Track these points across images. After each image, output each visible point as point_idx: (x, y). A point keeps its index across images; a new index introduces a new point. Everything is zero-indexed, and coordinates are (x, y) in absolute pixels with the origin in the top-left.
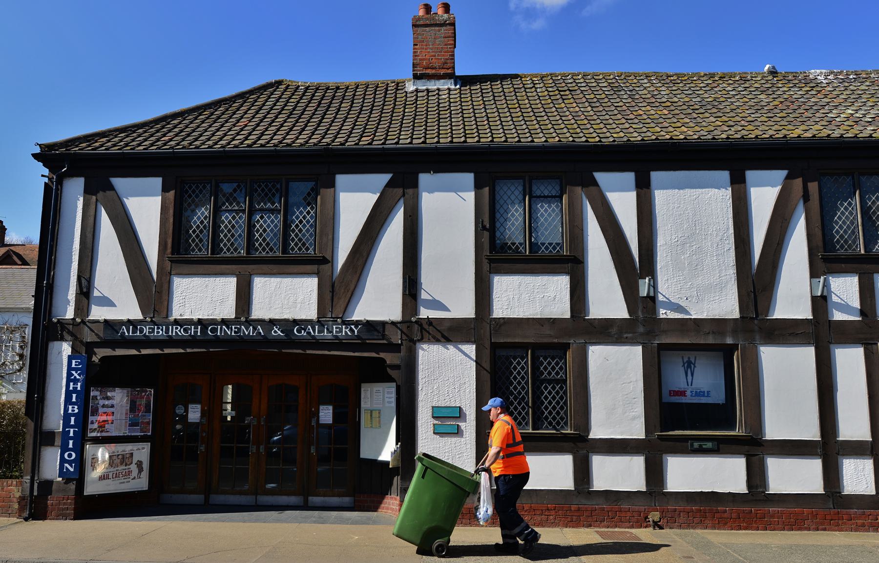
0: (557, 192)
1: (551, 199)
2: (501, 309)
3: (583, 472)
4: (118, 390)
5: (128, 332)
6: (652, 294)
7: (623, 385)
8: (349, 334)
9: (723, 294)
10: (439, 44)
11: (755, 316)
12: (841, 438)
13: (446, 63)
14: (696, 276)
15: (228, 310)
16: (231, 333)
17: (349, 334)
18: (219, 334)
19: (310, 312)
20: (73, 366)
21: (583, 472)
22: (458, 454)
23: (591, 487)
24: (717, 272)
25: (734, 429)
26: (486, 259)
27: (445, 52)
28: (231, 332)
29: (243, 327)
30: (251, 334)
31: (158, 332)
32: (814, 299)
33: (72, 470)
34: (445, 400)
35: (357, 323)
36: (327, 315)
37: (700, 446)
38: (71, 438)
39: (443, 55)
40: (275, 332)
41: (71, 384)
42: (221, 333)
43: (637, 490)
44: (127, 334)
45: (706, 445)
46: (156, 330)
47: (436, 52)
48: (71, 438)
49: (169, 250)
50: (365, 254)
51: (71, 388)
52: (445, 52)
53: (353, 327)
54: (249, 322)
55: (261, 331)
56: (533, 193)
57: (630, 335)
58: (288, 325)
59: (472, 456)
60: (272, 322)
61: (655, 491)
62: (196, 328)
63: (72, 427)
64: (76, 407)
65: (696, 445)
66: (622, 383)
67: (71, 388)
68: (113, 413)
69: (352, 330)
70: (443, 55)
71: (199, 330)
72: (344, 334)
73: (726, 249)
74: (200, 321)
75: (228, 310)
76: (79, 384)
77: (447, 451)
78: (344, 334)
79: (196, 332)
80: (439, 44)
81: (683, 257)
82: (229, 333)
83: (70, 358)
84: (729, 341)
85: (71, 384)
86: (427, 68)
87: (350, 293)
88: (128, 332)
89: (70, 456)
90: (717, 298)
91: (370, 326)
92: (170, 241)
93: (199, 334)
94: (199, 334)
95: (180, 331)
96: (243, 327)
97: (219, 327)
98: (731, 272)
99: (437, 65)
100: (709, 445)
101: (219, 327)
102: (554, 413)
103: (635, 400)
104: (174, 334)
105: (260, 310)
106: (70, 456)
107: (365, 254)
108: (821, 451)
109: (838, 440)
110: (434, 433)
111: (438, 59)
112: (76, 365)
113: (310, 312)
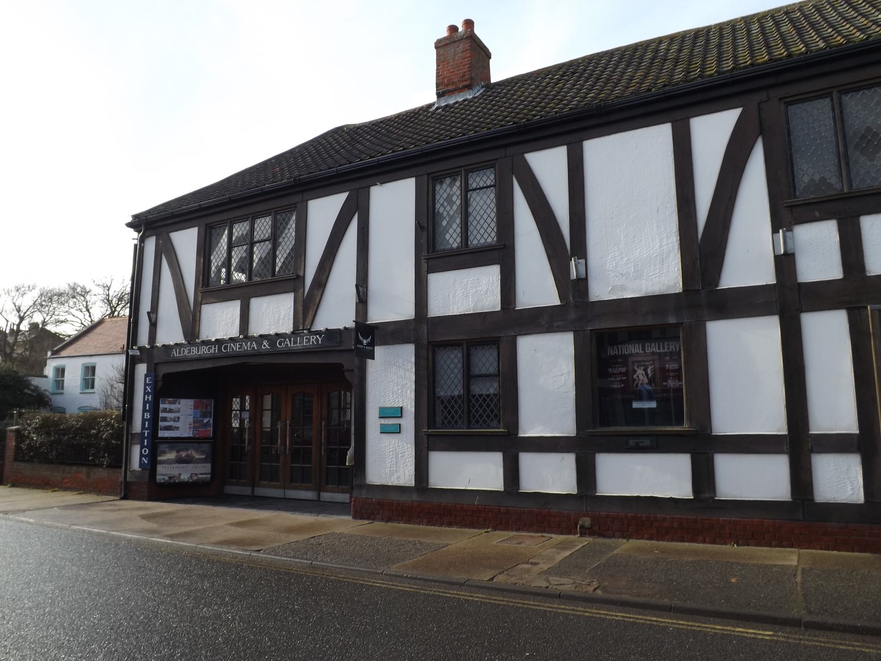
0: (492, 181)
1: (486, 189)
2: (437, 308)
3: (512, 473)
4: (183, 401)
5: (176, 354)
6: (583, 275)
7: (555, 378)
8: (315, 343)
9: (664, 265)
10: (458, 60)
11: (701, 288)
12: (814, 431)
13: (463, 76)
14: (634, 249)
15: (233, 331)
16: (236, 349)
17: (315, 343)
18: (228, 351)
19: (287, 327)
20: (147, 382)
21: (512, 473)
22: (400, 453)
23: (520, 488)
24: (658, 241)
25: (680, 422)
26: (424, 259)
27: (463, 66)
28: (236, 347)
29: (243, 343)
30: (249, 349)
31: (193, 352)
32: (778, 259)
33: (146, 462)
34: (390, 401)
35: (319, 333)
36: (299, 328)
37: (637, 444)
38: (146, 438)
39: (462, 69)
40: (264, 346)
41: (146, 396)
42: (230, 350)
43: (566, 493)
44: (289, 345)
45: (643, 442)
46: (192, 351)
47: (455, 68)
48: (146, 438)
49: (201, 285)
50: (328, 270)
51: (146, 399)
52: (463, 66)
53: (318, 336)
54: (252, 339)
55: (255, 346)
56: (469, 186)
57: (561, 323)
58: (273, 339)
59: (412, 455)
60: (262, 337)
61: (586, 495)
62: (215, 347)
63: (146, 429)
64: (149, 414)
65: (632, 442)
66: (553, 376)
67: (146, 399)
68: (179, 418)
69: (317, 340)
70: (462, 69)
71: (217, 348)
72: (311, 344)
73: (667, 214)
74: (218, 341)
75: (233, 331)
76: (150, 396)
77: (391, 450)
78: (311, 344)
79: (215, 350)
80: (458, 60)
81: (618, 230)
82: (235, 349)
83: (146, 376)
84: (672, 320)
85: (146, 396)
86: (447, 85)
87: (316, 306)
88: (176, 354)
89: (145, 451)
90: (658, 271)
91: (330, 334)
92: (201, 278)
93: (217, 352)
94: (217, 352)
95: (205, 350)
96: (243, 343)
97: (229, 345)
98: (673, 240)
99: (456, 80)
100: (647, 442)
101: (229, 345)
102: (488, 411)
103: (567, 394)
104: (202, 353)
105: (257, 328)
106: (145, 451)
107: (328, 270)
108: (787, 448)
109: (811, 434)
110: (400, 432)
111: (457, 74)
112: (149, 381)
113: (287, 327)
